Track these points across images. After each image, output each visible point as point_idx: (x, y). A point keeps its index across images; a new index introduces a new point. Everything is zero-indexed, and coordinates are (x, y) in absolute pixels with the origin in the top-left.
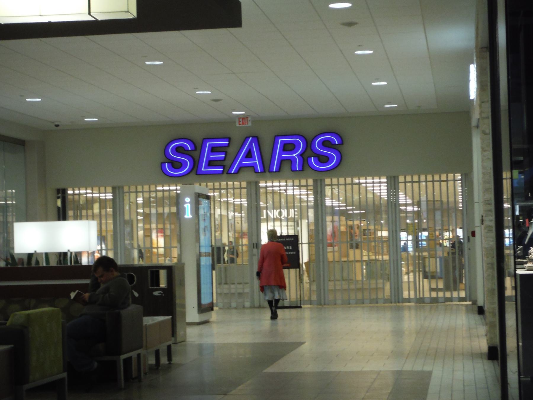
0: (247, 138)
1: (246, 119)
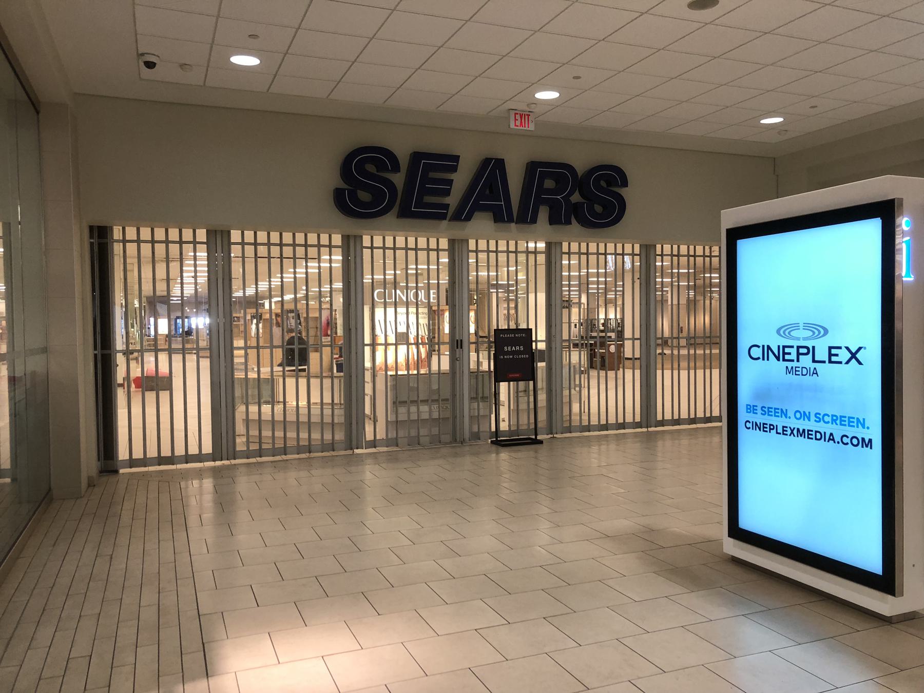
1: (526, 117)
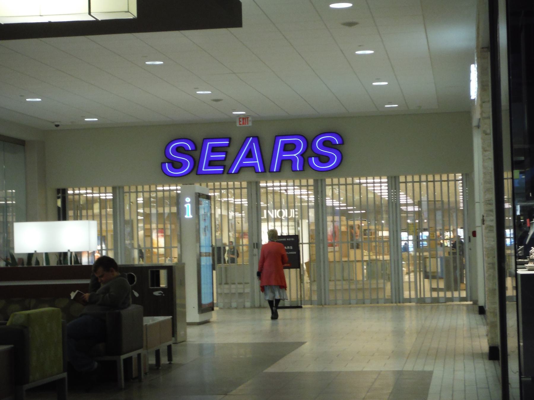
0: (248, 138)
1: (246, 119)
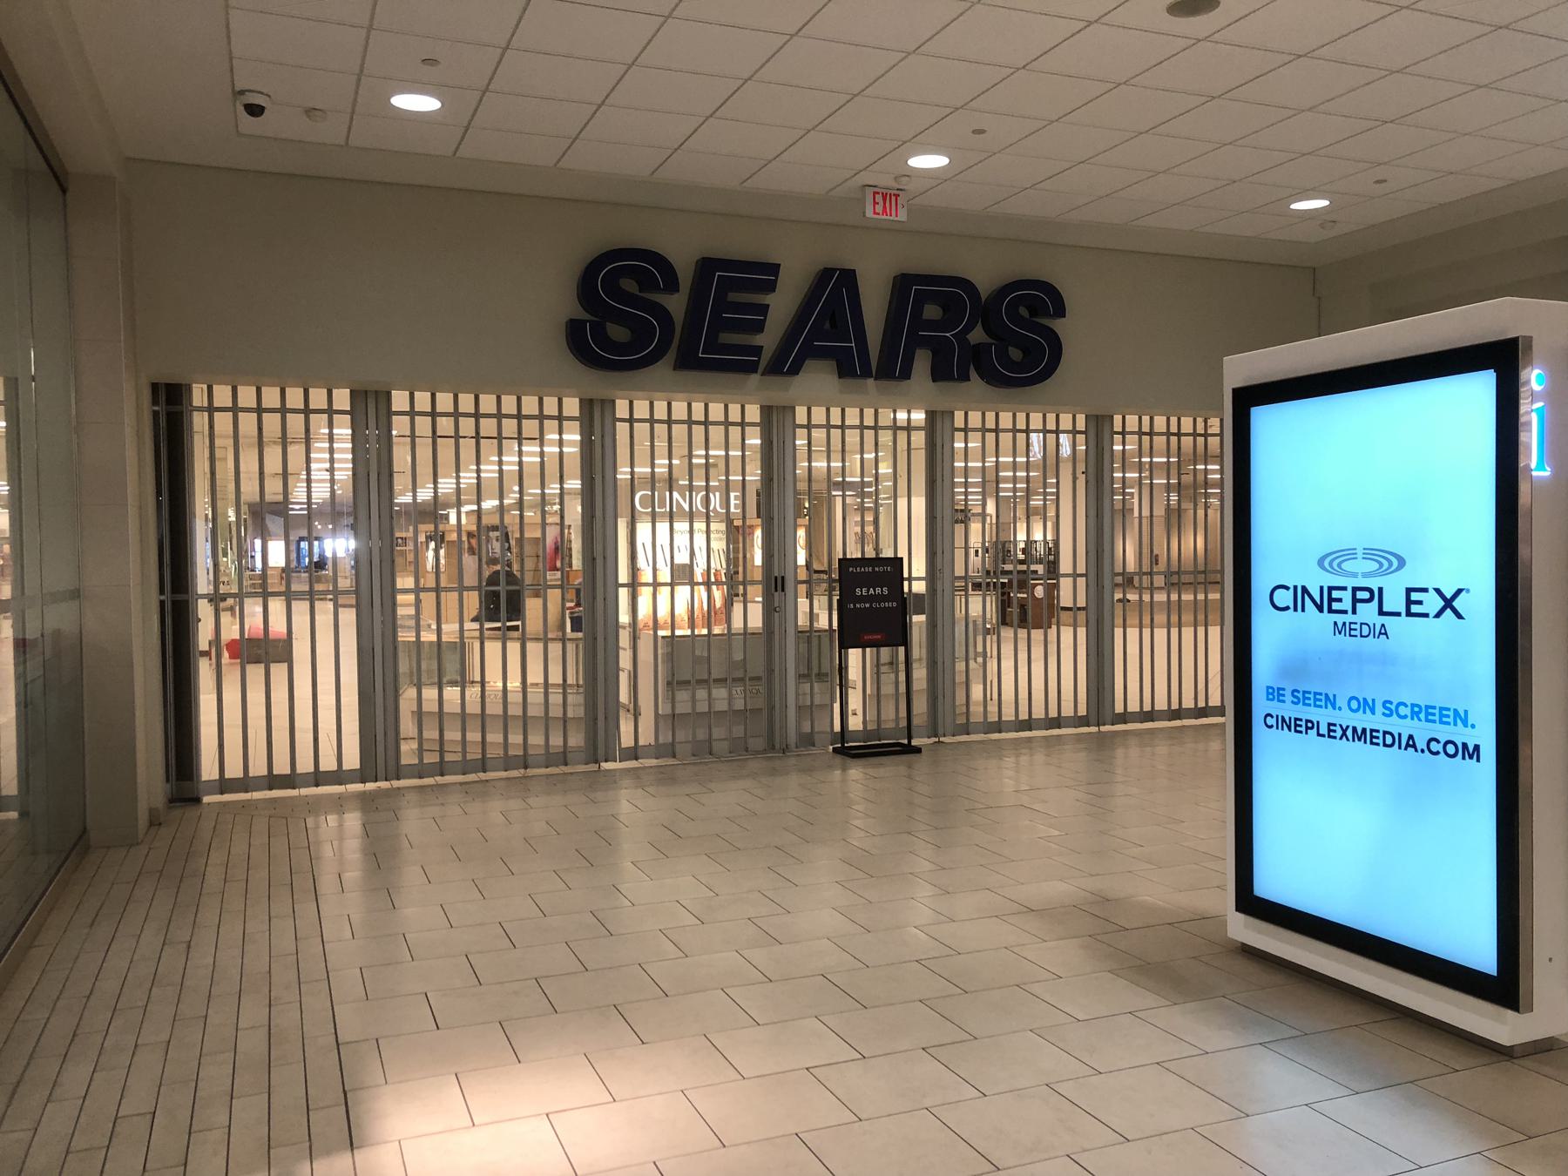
1: (893, 198)
